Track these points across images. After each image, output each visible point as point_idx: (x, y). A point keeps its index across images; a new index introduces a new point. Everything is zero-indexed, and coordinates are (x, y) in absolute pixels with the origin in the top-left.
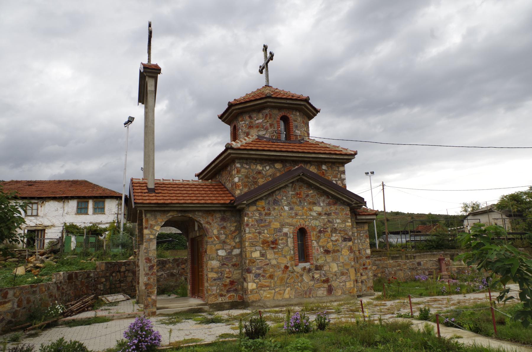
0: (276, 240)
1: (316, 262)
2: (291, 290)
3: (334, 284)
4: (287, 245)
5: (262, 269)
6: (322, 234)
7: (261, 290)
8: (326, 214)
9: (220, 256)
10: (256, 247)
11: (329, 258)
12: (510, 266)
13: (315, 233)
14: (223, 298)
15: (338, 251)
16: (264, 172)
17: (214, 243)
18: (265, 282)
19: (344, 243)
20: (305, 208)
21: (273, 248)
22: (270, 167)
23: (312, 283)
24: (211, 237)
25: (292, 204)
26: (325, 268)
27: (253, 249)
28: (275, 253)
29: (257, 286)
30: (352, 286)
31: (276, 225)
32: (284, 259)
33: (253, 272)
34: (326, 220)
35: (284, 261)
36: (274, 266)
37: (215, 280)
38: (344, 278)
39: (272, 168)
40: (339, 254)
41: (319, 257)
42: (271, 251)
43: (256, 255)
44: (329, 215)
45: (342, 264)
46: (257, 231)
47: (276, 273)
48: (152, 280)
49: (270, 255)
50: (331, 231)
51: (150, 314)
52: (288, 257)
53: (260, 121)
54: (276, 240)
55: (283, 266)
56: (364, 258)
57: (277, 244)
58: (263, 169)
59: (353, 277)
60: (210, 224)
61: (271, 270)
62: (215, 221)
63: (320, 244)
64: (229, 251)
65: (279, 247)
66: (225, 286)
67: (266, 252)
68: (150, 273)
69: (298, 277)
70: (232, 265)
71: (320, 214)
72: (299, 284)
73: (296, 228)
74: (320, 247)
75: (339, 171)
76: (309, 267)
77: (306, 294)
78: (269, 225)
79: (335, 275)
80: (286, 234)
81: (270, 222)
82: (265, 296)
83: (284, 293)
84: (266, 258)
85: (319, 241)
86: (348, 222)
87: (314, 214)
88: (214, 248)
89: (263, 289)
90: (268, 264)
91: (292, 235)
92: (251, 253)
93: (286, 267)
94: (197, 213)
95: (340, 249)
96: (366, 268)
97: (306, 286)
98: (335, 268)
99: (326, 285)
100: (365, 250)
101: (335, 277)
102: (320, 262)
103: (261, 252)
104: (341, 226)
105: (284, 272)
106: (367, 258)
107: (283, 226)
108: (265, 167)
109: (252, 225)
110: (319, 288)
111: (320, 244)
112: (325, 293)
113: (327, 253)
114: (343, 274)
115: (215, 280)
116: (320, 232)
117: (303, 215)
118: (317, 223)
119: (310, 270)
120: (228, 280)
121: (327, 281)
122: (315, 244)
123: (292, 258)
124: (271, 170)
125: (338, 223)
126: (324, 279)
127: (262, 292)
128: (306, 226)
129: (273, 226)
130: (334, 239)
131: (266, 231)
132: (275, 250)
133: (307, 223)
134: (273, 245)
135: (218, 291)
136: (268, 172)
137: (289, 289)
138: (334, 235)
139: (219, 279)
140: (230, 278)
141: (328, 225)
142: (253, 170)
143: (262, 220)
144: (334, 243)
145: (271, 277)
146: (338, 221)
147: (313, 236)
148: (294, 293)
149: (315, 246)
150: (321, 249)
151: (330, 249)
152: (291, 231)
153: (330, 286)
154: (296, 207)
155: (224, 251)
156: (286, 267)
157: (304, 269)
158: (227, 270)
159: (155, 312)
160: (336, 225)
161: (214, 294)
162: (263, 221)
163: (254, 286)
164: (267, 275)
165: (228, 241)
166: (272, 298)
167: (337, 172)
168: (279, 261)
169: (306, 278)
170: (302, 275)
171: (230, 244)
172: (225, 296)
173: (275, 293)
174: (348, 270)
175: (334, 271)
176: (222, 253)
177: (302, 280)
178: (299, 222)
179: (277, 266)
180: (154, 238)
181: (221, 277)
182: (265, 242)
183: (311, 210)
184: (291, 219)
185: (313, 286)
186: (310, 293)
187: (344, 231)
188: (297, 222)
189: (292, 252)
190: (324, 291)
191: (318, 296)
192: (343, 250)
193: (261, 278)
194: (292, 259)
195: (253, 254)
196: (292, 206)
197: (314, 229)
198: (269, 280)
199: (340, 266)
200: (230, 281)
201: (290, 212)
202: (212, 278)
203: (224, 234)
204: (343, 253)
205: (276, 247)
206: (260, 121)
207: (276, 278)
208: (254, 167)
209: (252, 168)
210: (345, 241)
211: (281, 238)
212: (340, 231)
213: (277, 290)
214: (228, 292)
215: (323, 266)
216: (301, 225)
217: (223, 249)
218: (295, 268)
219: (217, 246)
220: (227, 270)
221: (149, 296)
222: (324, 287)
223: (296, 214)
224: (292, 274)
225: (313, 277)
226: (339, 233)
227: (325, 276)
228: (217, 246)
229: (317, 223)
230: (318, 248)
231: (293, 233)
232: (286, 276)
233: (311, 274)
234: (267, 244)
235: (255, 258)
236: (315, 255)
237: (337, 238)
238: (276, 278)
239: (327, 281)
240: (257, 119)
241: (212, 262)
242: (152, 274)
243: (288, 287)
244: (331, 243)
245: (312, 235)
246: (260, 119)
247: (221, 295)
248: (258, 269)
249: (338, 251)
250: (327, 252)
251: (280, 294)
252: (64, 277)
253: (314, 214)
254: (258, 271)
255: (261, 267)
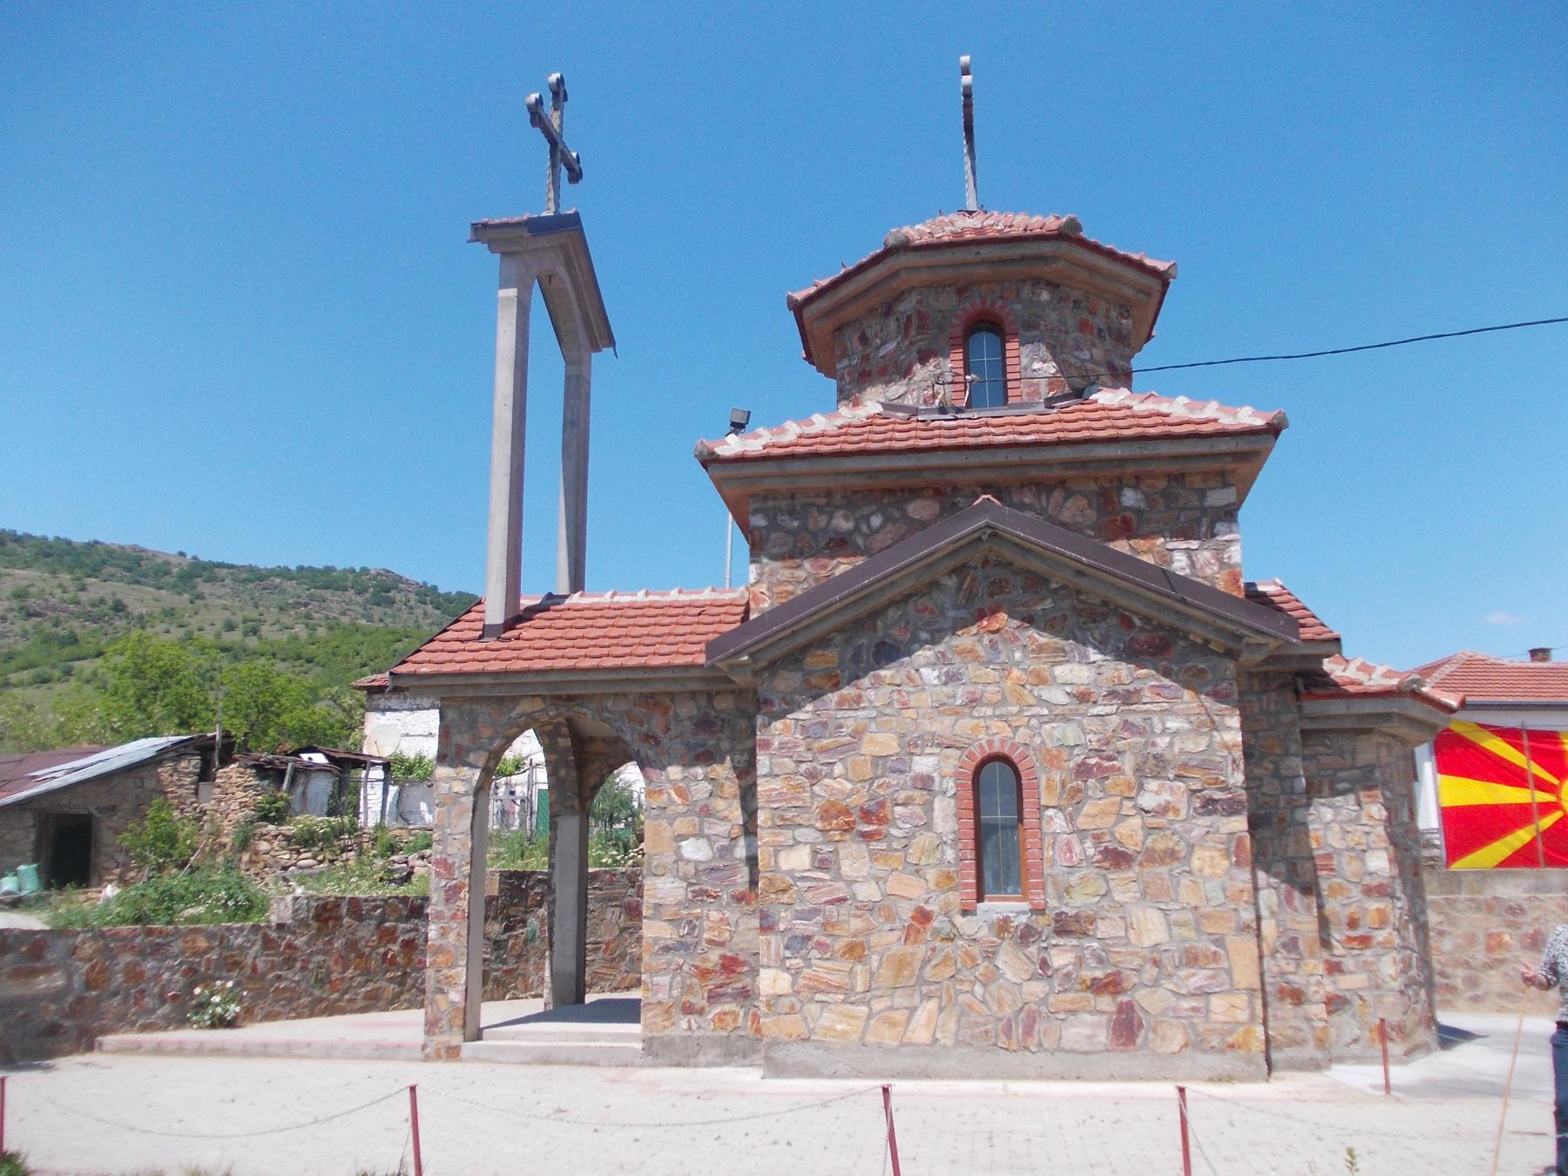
0: (881, 805)
1: (1060, 898)
2: (941, 1009)
3: (1148, 1001)
4: (928, 826)
5: (820, 918)
6: (1091, 781)
7: (810, 1000)
8: (1112, 694)
9: (688, 861)
10: (798, 832)
11: (1124, 886)
12: (413, 934)
13: (1057, 777)
14: (693, 1018)
15: (1172, 855)
16: (860, 541)
17: (671, 810)
18: (830, 971)
19: (1206, 821)
20: (1016, 673)
21: (867, 837)
22: (888, 519)
23: (1038, 988)
24: (661, 792)
25: (957, 659)
26: (1103, 929)
27: (785, 836)
28: (874, 856)
29: (794, 983)
30: (1243, 1016)
31: (883, 742)
32: (914, 879)
33: (782, 927)
34: (1115, 720)
35: (913, 891)
36: (870, 908)
37: (666, 949)
38: (1199, 978)
39: (895, 521)
40: (1178, 868)
41: (1074, 879)
42: (861, 848)
43: (797, 860)
44: (1129, 698)
45: (1189, 916)
46: (803, 767)
47: (874, 939)
48: (452, 937)
49: (854, 860)
50: (1138, 770)
51: (443, 1052)
52: (931, 874)
53: (891, 346)
54: (881, 805)
55: (906, 912)
56: (1356, 892)
57: (883, 821)
58: (857, 529)
59: (1246, 975)
60: (658, 742)
61: (856, 924)
62: (673, 733)
63: (1082, 822)
64: (725, 842)
65: (894, 831)
66: (704, 974)
67: (836, 852)
68: (448, 914)
69: (973, 959)
70: (733, 897)
71: (1083, 697)
72: (978, 989)
73: (971, 756)
74: (1082, 833)
75: (1204, 510)
76: (1024, 919)
77: (1008, 1032)
78: (852, 746)
79: (1156, 963)
80: (925, 783)
81: (857, 734)
82: (829, 1029)
83: (908, 1021)
84: (838, 876)
85: (1078, 811)
86: (1229, 728)
87: (1058, 696)
88: (668, 833)
89: (819, 997)
90: (844, 900)
91: (950, 785)
92: (776, 853)
93: (923, 916)
94: (610, 704)
95: (1182, 848)
96: (1365, 941)
97: (1008, 998)
98: (1151, 929)
99: (1106, 1003)
100: (1361, 853)
101: (1150, 972)
102: (1077, 903)
103: (815, 852)
104: (1190, 746)
105: (910, 934)
106: (1368, 891)
107: (911, 746)
108: (867, 518)
109: (782, 746)
110: (1073, 1012)
111: (1082, 822)
112: (1103, 1037)
113: (1117, 865)
114: (1192, 959)
115: (666, 949)
116: (1083, 771)
117: (1003, 701)
118: (1069, 733)
119: (1027, 935)
120: (714, 956)
121: (1111, 985)
122: (1057, 822)
123: (949, 877)
124: (889, 526)
125: (1176, 733)
126: (1099, 974)
127: (814, 1008)
128: (1014, 746)
129: (868, 748)
130: (1148, 800)
131: (838, 769)
132: (874, 845)
133: (1022, 736)
134: (869, 823)
135: (676, 993)
136: (879, 536)
137: (932, 1005)
138: (1153, 785)
139: (682, 946)
140: (721, 944)
141: (1120, 745)
142: (814, 534)
143: (824, 725)
144: (1152, 821)
145: (856, 951)
146: (1173, 724)
147: (1049, 787)
148: (952, 1025)
149: (1057, 832)
150: (1088, 844)
151: (1130, 847)
152: (950, 767)
153: (1126, 1010)
154: (972, 671)
155: (702, 842)
156: (923, 916)
157: (1003, 926)
158: (715, 915)
159: (458, 1048)
160: (1163, 742)
161: (660, 1003)
162: (831, 727)
163: (784, 982)
164: (840, 944)
165: (720, 804)
166: (856, 1037)
167: (1197, 514)
168: (891, 887)
169: (1011, 964)
170: (990, 955)
171: (725, 819)
172: (701, 1012)
173: (869, 1017)
174: (1219, 941)
175: (1147, 944)
176: (695, 851)
177: (993, 976)
178: (989, 732)
179: (881, 909)
180: (466, 794)
181: (689, 939)
182: (831, 812)
183: (1041, 680)
184: (948, 720)
185: (1044, 1001)
186: (1028, 1032)
187: (1205, 766)
188: (975, 729)
189: (950, 854)
190: (1094, 1026)
191: (1065, 1044)
192: (1198, 853)
193: (814, 953)
194: (948, 881)
195: (782, 855)
196: (953, 669)
197: (1052, 760)
198: (846, 965)
199: (1180, 925)
200: (723, 957)
201: (948, 689)
202: (656, 940)
203: (706, 778)
204: (1196, 863)
205: (878, 832)
206: (891, 346)
207: (875, 958)
208: (822, 521)
209: (811, 525)
210: (1209, 813)
211: (902, 796)
212: (1185, 766)
213: (878, 1005)
214: (714, 997)
215: (1092, 920)
216: (990, 743)
217: (699, 835)
218: (959, 920)
219: (681, 825)
220: (715, 915)
221: (442, 991)
222: (1096, 1012)
223: (974, 702)
224: (949, 948)
225: (1044, 964)
226: (1178, 777)
227: (1101, 961)
228: (681, 825)
229: (1069, 733)
230: (1074, 838)
231: (957, 776)
232: (921, 951)
233: (1033, 949)
234: (842, 820)
235: (790, 872)
236: (1057, 870)
237: (1166, 797)
238: (875, 958)
239: (1111, 985)
240: (884, 343)
241: (659, 882)
242: (454, 917)
243: (929, 997)
244: (1136, 822)
245: (1045, 785)
246: (892, 339)
247: (688, 1010)
248: (801, 915)
249: (1172, 855)
250: (1116, 858)
251: (893, 1024)
252: (295, 911)
253: (1058, 696)
254: (802, 927)
255: (815, 912)
